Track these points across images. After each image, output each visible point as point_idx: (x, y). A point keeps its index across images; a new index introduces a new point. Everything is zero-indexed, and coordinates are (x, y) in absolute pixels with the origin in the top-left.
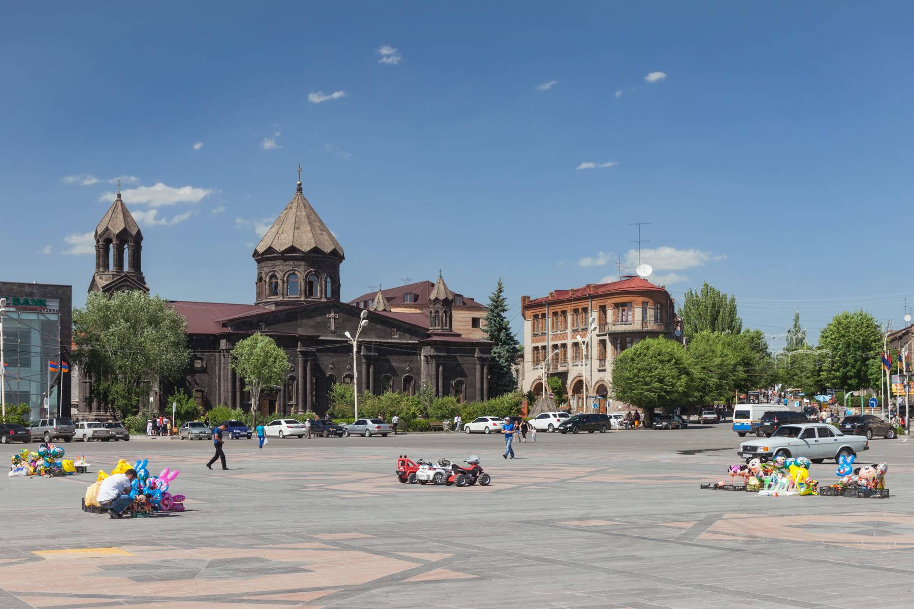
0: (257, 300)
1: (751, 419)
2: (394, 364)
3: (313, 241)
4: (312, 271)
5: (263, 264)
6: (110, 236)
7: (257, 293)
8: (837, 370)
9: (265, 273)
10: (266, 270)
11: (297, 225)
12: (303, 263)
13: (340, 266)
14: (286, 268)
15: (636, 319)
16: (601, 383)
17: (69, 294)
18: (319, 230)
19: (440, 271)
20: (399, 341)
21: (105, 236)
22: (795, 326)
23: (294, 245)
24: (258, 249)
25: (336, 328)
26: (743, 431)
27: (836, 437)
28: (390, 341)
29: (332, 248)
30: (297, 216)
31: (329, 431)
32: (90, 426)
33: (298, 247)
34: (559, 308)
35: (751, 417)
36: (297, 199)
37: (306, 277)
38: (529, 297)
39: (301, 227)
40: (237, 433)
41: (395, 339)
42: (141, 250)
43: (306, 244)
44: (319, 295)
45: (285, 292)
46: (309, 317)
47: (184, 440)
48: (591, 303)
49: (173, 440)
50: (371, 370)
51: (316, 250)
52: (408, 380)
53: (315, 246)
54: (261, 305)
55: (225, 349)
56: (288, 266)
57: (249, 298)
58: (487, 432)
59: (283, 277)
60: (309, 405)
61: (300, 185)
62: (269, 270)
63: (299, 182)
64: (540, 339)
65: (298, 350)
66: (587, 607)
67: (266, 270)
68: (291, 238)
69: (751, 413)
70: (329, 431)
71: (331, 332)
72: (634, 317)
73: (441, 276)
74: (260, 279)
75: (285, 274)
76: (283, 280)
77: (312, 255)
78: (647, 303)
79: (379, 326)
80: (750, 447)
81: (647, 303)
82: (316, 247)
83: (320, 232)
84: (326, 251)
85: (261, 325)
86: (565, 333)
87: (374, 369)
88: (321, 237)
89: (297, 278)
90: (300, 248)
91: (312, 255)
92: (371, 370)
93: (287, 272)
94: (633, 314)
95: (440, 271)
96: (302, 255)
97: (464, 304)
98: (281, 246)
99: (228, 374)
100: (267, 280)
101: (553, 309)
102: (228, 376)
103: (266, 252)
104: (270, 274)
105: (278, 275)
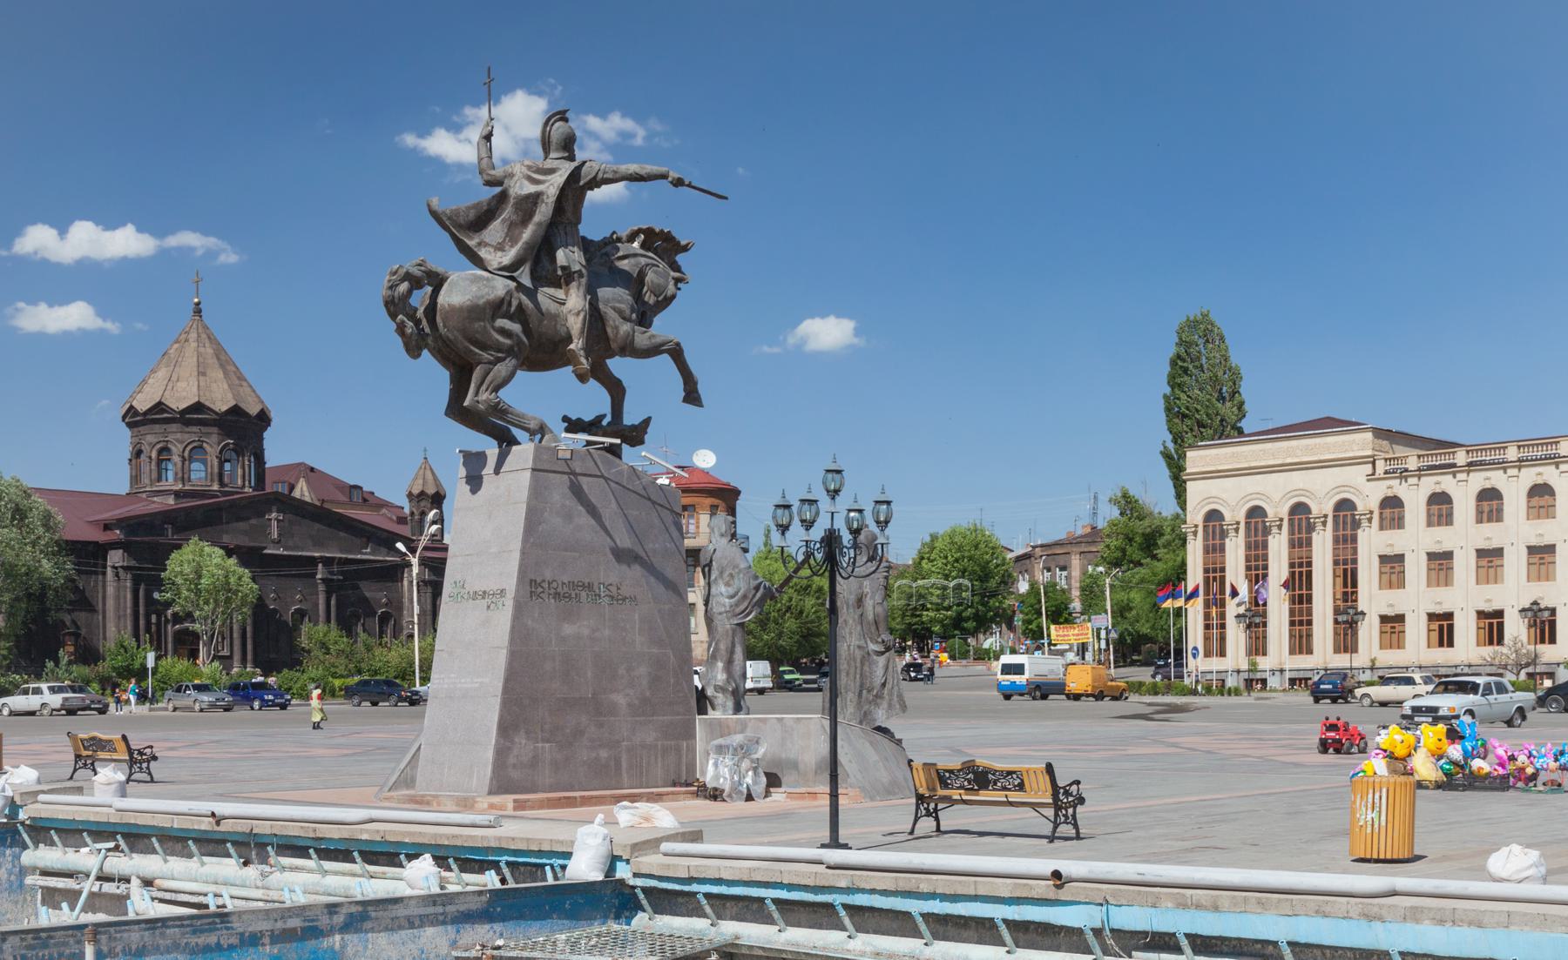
0: (131, 487)
1: (1027, 675)
2: (368, 594)
3: (230, 396)
4: (228, 444)
7: (131, 476)
8: (949, 608)
9: (150, 444)
10: (151, 438)
12: (215, 430)
13: (265, 435)
14: (188, 438)
15: (701, 530)
18: (235, 379)
20: (372, 558)
22: (766, 544)
23: (202, 401)
24: (135, 404)
25: (279, 535)
26: (1008, 692)
27: (1510, 694)
28: (359, 557)
30: (199, 355)
31: (263, 700)
32: (52, 690)
33: (207, 403)
35: (1027, 672)
36: (194, 326)
37: (221, 452)
39: (209, 372)
40: (270, 701)
41: (366, 554)
43: (221, 401)
44: (240, 482)
45: (186, 476)
46: (240, 519)
47: (177, 713)
49: (152, 713)
50: (333, 602)
51: (236, 411)
52: (385, 619)
53: (234, 403)
54: (144, 496)
55: (122, 567)
56: (191, 435)
57: (122, 486)
60: (249, 657)
61: (198, 304)
62: (156, 440)
63: (196, 300)
66: (1164, 942)
68: (195, 389)
69: (1026, 667)
70: (263, 700)
71: (273, 542)
72: (698, 527)
73: (426, 458)
74: (138, 453)
75: (186, 446)
76: (183, 457)
77: (229, 418)
78: (717, 507)
79: (342, 534)
80: (1427, 707)
81: (717, 507)
82: (236, 406)
83: (237, 382)
84: (251, 413)
85: (167, 529)
87: (338, 600)
88: (240, 389)
89: (206, 452)
90: (212, 406)
91: (229, 418)
92: (333, 602)
93: (189, 444)
94: (698, 523)
95: (425, 450)
96: (214, 416)
97: (365, 500)
98: (180, 400)
99: (125, 607)
100: (154, 455)
102: (125, 611)
103: (150, 411)
104: (159, 446)
105: (173, 448)
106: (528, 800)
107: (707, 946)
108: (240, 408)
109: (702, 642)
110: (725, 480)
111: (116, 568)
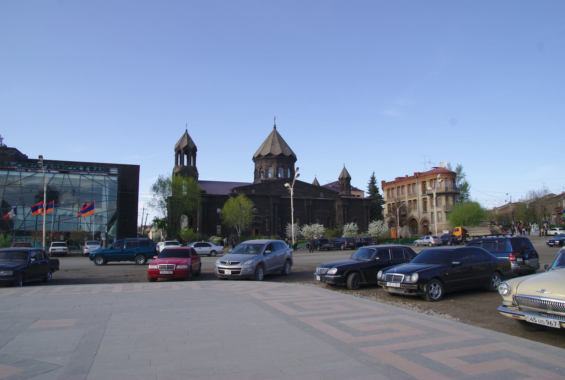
3: (280, 150)
5: (257, 163)
6: (180, 149)
11: (273, 143)
15: (442, 186)
16: (424, 219)
17: (138, 170)
19: (344, 164)
21: (178, 149)
23: (271, 152)
29: (290, 154)
33: (273, 153)
34: (400, 184)
38: (385, 181)
42: (196, 156)
45: (267, 176)
48: (418, 180)
51: (282, 155)
53: (281, 152)
58: (430, 245)
59: (266, 168)
62: (259, 166)
64: (391, 200)
65: (271, 202)
67: (258, 165)
68: (270, 150)
75: (267, 167)
82: (282, 153)
83: (284, 147)
84: (287, 155)
86: (404, 197)
93: (268, 166)
95: (344, 164)
100: (259, 170)
101: (397, 185)
106: (395, 243)
107: (440, 304)
108: (283, 154)
109: (444, 225)
110: (365, 300)
111: (338, 206)
